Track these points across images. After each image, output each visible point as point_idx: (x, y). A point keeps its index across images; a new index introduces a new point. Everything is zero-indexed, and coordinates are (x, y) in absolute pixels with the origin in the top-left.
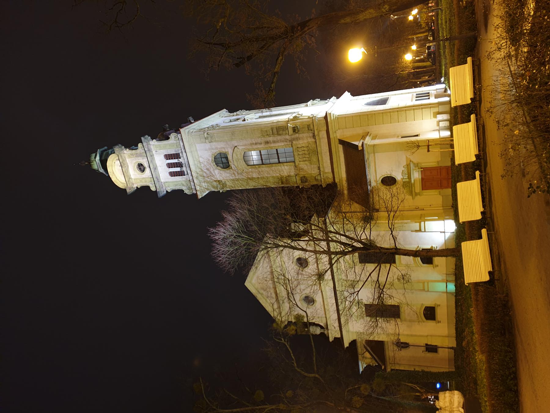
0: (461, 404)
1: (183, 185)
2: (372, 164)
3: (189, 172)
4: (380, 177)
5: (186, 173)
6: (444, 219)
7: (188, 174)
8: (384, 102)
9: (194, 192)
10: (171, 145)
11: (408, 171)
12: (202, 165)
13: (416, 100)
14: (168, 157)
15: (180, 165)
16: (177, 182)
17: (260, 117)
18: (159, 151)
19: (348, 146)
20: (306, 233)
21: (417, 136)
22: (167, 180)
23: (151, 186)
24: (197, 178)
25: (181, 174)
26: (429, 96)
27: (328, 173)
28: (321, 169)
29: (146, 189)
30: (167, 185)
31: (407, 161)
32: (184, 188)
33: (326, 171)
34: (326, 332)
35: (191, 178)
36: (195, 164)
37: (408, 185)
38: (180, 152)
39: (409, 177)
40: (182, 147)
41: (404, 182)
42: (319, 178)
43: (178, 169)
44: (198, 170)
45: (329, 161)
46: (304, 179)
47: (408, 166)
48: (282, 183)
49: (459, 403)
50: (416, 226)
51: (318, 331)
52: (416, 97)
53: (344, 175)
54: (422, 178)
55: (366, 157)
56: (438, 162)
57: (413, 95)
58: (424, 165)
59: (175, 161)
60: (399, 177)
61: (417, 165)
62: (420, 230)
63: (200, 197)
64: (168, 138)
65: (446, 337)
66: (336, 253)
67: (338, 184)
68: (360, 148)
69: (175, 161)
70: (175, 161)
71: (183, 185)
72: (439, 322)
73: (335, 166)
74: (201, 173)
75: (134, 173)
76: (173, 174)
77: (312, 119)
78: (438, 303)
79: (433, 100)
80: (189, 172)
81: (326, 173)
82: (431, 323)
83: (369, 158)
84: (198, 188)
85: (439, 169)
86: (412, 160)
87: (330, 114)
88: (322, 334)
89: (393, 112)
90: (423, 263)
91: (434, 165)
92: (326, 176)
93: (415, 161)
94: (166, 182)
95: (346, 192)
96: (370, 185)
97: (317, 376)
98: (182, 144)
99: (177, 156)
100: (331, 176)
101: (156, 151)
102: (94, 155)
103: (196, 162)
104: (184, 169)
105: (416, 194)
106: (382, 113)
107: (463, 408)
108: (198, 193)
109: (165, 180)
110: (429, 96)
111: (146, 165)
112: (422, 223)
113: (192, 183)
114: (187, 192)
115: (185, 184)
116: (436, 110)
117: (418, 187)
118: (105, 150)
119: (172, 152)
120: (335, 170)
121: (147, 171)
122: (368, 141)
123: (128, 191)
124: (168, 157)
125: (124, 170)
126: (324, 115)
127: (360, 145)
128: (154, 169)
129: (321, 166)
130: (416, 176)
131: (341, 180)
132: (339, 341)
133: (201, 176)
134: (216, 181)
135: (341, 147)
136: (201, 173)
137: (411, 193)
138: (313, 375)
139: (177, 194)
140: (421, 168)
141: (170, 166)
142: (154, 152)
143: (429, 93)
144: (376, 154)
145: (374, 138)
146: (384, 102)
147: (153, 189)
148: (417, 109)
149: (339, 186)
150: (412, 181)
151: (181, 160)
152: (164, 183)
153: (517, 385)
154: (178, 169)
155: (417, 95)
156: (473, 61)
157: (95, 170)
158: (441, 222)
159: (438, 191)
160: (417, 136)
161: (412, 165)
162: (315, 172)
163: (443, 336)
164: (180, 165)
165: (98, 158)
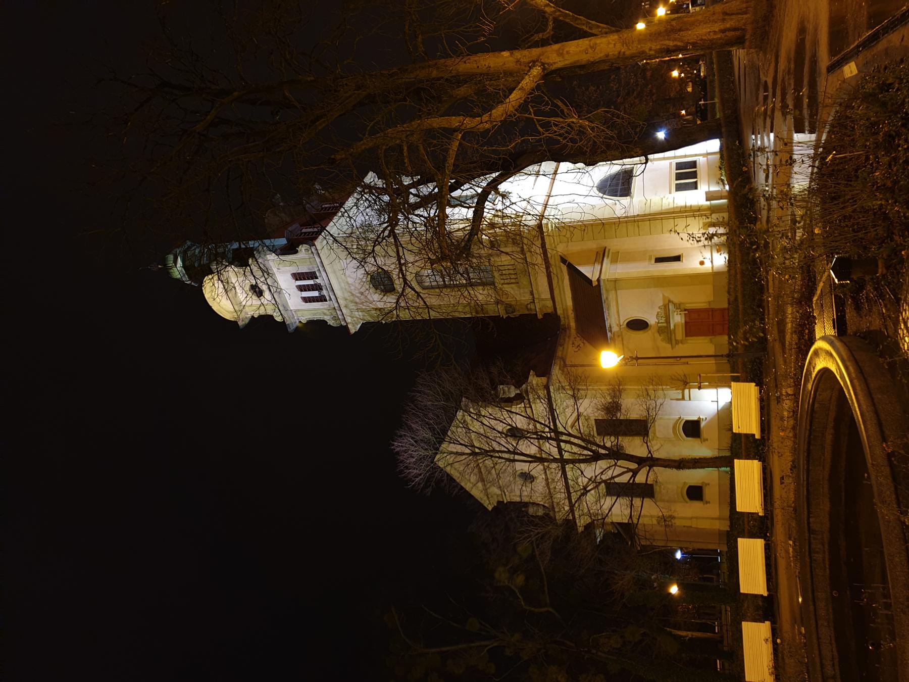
1: (325, 314)
2: (613, 309)
3: (333, 297)
4: (624, 320)
5: (328, 298)
6: (716, 387)
7: (331, 299)
9: (343, 323)
10: (302, 259)
11: (665, 313)
12: (353, 288)
14: (297, 276)
15: (318, 287)
16: (314, 310)
18: (283, 269)
20: (519, 398)
21: (677, 258)
22: (299, 308)
23: (275, 314)
24: (346, 306)
25: (322, 299)
27: (546, 300)
28: (536, 296)
29: (266, 320)
30: (299, 314)
31: (664, 300)
32: (326, 318)
33: (543, 297)
34: (551, 513)
35: (336, 305)
36: (342, 288)
37: (665, 331)
38: (316, 270)
39: (668, 321)
40: (319, 264)
41: (659, 327)
42: (532, 306)
43: (315, 294)
44: (347, 295)
45: (546, 284)
46: (509, 307)
47: (666, 307)
48: (477, 312)
50: (677, 394)
51: (541, 512)
53: (569, 302)
54: (686, 323)
55: (604, 297)
56: (709, 302)
57: (671, 164)
58: (688, 306)
59: (311, 282)
60: (652, 320)
61: (678, 306)
62: (683, 399)
63: (353, 331)
64: (296, 252)
65: (716, 519)
66: (573, 462)
67: (561, 316)
68: (595, 284)
69: (311, 282)
70: (307, 280)
71: (325, 314)
72: (707, 502)
73: (556, 292)
74: (352, 298)
75: (242, 295)
76: (306, 300)
78: (707, 482)
80: (333, 297)
81: (543, 300)
82: (697, 504)
84: (349, 320)
85: (710, 312)
86: (672, 299)
88: (547, 515)
89: (643, 221)
90: (687, 436)
91: (704, 306)
92: (543, 303)
93: (676, 300)
94: (299, 310)
95: (573, 324)
96: (611, 331)
97: (551, 610)
98: (318, 260)
99: (312, 275)
100: (549, 304)
101: (282, 272)
102: (171, 257)
103: (343, 285)
104: (324, 292)
105: (677, 342)
106: (626, 222)
108: (350, 326)
109: (295, 307)
112: (687, 391)
113: (339, 312)
114: (331, 323)
115: (328, 313)
117: (680, 334)
118: (189, 248)
119: (304, 269)
120: (556, 300)
121: (267, 294)
123: (240, 323)
125: (229, 297)
128: (276, 291)
129: (535, 291)
130: (678, 319)
131: (565, 310)
132: (570, 524)
133: (352, 302)
134: (376, 309)
136: (352, 298)
137: (670, 341)
138: (546, 609)
139: (316, 326)
140: (685, 310)
141: (301, 288)
142: (275, 270)
144: (619, 292)
147: (279, 319)
148: (679, 217)
149: (562, 319)
150: (672, 327)
151: (318, 281)
152: (296, 311)
154: (315, 294)
156: (762, 400)
157: (178, 280)
158: (713, 391)
159: (709, 338)
160: (677, 258)
161: (671, 307)
162: (526, 298)
163: (712, 519)
164: (318, 287)
165: (179, 263)
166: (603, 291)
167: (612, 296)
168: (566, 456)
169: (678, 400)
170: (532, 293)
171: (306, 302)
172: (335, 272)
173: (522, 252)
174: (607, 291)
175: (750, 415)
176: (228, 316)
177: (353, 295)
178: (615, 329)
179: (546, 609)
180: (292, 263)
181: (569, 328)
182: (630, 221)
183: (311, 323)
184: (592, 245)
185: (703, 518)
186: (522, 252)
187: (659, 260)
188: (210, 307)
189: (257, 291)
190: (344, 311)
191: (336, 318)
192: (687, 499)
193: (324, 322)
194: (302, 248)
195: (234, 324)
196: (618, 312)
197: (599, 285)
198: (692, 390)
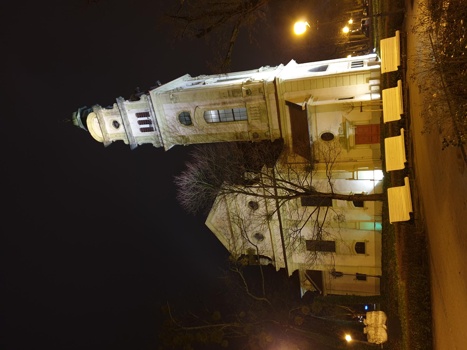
0: (385, 322)
1: (152, 140)
2: (314, 123)
3: (157, 128)
4: (320, 133)
5: (154, 129)
7: (156, 130)
8: (324, 69)
12: (168, 122)
13: (352, 67)
14: (139, 115)
16: (146, 136)
17: (218, 81)
18: (131, 110)
19: (293, 107)
20: (257, 180)
21: (352, 98)
22: (138, 135)
23: (124, 140)
24: (164, 133)
25: (150, 130)
26: (363, 64)
27: (276, 130)
28: (271, 127)
29: (120, 142)
30: (138, 139)
32: (153, 142)
33: (275, 128)
34: (273, 263)
35: (159, 133)
36: (162, 122)
37: (344, 140)
38: (149, 111)
39: (345, 134)
40: (151, 106)
41: (340, 138)
42: (268, 134)
43: (148, 126)
44: (165, 127)
45: (277, 120)
46: (256, 135)
47: (344, 124)
48: (237, 138)
49: (383, 321)
50: (350, 175)
51: (267, 262)
52: (352, 65)
53: (290, 132)
56: (369, 120)
57: (349, 63)
59: (145, 119)
60: (336, 133)
61: (351, 123)
62: (353, 179)
64: (138, 99)
65: (373, 267)
67: (285, 139)
68: (304, 109)
69: (145, 119)
71: (152, 140)
72: (368, 255)
74: (168, 129)
76: (143, 130)
77: (263, 83)
79: (366, 67)
80: (157, 128)
81: (275, 130)
82: (361, 256)
83: (312, 117)
87: (278, 79)
88: (270, 265)
89: (332, 77)
90: (356, 206)
93: (350, 119)
95: (291, 146)
96: (312, 140)
97: (265, 299)
98: (151, 104)
99: (146, 114)
100: (278, 132)
101: (130, 110)
103: (163, 120)
104: (153, 125)
105: (351, 148)
107: (386, 325)
108: (165, 146)
109: (137, 135)
110: (363, 64)
111: (120, 122)
112: (355, 173)
113: (160, 138)
114: (155, 145)
116: (369, 76)
117: (352, 142)
122: (310, 102)
123: (105, 144)
124: (139, 115)
126: (273, 79)
127: (304, 106)
130: (351, 132)
131: (287, 136)
132: (284, 270)
133: (167, 132)
134: (180, 136)
135: (287, 108)
136: (168, 129)
138: (262, 299)
139: (147, 147)
140: (355, 126)
141: (140, 123)
142: (127, 111)
143: (362, 61)
145: (316, 100)
146: (324, 69)
147: (126, 143)
148: (352, 75)
149: (285, 141)
150: (348, 137)
151: (150, 118)
152: (136, 137)
153: (430, 305)
154: (148, 126)
155: (352, 63)
157: (76, 126)
158: (371, 172)
159: (369, 145)
160: (352, 98)
161: (347, 123)
162: (265, 129)
163: (371, 267)
164: (149, 122)
166: (308, 113)
167: (313, 117)
168: (279, 195)
169: (350, 179)
170: (268, 126)
171: (142, 132)
172: (159, 111)
173: (264, 98)
174: (311, 113)
175: (393, 54)
176: (99, 140)
177: (168, 127)
178: (314, 139)
179: (262, 299)
180: (136, 107)
181: (289, 148)
182: (325, 78)
183: (144, 145)
184: (304, 94)
185: (365, 267)
186: (264, 98)
187: (339, 99)
188: (90, 134)
189: (116, 124)
190: (162, 136)
191: (158, 142)
192: (356, 253)
193: (151, 144)
194: (143, 97)
195: (102, 144)
196: (316, 128)
197: (306, 110)
198: (358, 172)
